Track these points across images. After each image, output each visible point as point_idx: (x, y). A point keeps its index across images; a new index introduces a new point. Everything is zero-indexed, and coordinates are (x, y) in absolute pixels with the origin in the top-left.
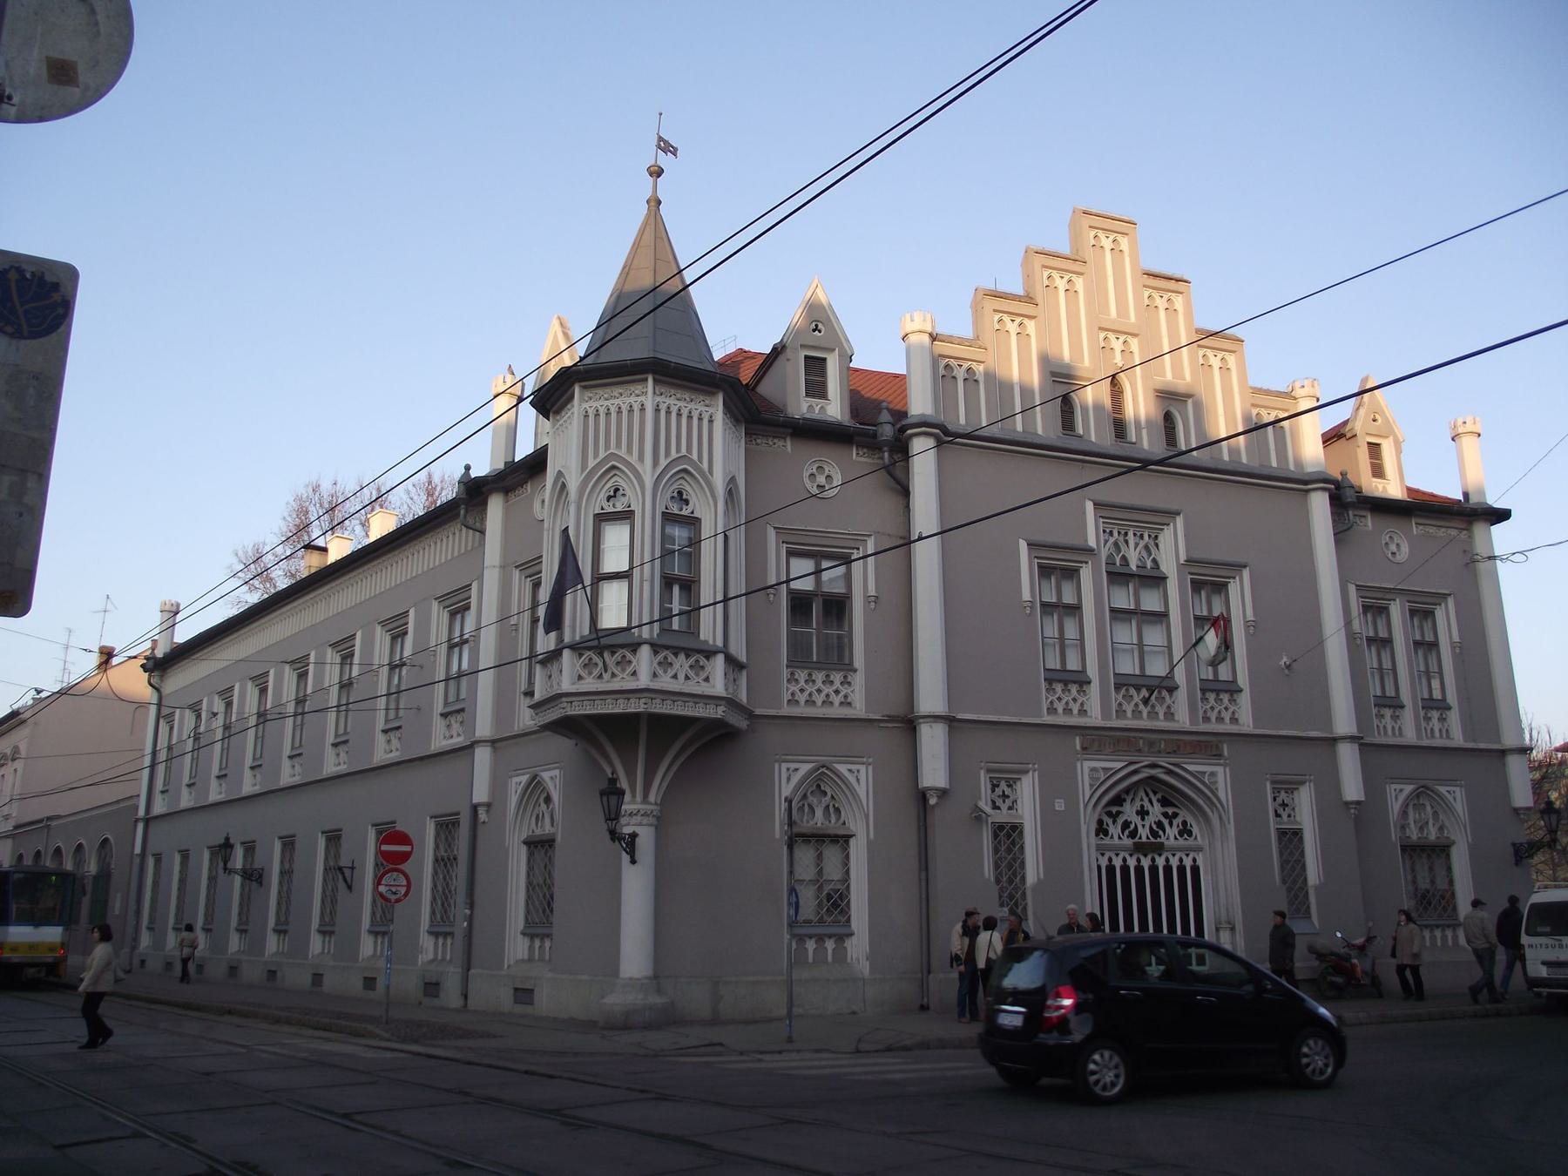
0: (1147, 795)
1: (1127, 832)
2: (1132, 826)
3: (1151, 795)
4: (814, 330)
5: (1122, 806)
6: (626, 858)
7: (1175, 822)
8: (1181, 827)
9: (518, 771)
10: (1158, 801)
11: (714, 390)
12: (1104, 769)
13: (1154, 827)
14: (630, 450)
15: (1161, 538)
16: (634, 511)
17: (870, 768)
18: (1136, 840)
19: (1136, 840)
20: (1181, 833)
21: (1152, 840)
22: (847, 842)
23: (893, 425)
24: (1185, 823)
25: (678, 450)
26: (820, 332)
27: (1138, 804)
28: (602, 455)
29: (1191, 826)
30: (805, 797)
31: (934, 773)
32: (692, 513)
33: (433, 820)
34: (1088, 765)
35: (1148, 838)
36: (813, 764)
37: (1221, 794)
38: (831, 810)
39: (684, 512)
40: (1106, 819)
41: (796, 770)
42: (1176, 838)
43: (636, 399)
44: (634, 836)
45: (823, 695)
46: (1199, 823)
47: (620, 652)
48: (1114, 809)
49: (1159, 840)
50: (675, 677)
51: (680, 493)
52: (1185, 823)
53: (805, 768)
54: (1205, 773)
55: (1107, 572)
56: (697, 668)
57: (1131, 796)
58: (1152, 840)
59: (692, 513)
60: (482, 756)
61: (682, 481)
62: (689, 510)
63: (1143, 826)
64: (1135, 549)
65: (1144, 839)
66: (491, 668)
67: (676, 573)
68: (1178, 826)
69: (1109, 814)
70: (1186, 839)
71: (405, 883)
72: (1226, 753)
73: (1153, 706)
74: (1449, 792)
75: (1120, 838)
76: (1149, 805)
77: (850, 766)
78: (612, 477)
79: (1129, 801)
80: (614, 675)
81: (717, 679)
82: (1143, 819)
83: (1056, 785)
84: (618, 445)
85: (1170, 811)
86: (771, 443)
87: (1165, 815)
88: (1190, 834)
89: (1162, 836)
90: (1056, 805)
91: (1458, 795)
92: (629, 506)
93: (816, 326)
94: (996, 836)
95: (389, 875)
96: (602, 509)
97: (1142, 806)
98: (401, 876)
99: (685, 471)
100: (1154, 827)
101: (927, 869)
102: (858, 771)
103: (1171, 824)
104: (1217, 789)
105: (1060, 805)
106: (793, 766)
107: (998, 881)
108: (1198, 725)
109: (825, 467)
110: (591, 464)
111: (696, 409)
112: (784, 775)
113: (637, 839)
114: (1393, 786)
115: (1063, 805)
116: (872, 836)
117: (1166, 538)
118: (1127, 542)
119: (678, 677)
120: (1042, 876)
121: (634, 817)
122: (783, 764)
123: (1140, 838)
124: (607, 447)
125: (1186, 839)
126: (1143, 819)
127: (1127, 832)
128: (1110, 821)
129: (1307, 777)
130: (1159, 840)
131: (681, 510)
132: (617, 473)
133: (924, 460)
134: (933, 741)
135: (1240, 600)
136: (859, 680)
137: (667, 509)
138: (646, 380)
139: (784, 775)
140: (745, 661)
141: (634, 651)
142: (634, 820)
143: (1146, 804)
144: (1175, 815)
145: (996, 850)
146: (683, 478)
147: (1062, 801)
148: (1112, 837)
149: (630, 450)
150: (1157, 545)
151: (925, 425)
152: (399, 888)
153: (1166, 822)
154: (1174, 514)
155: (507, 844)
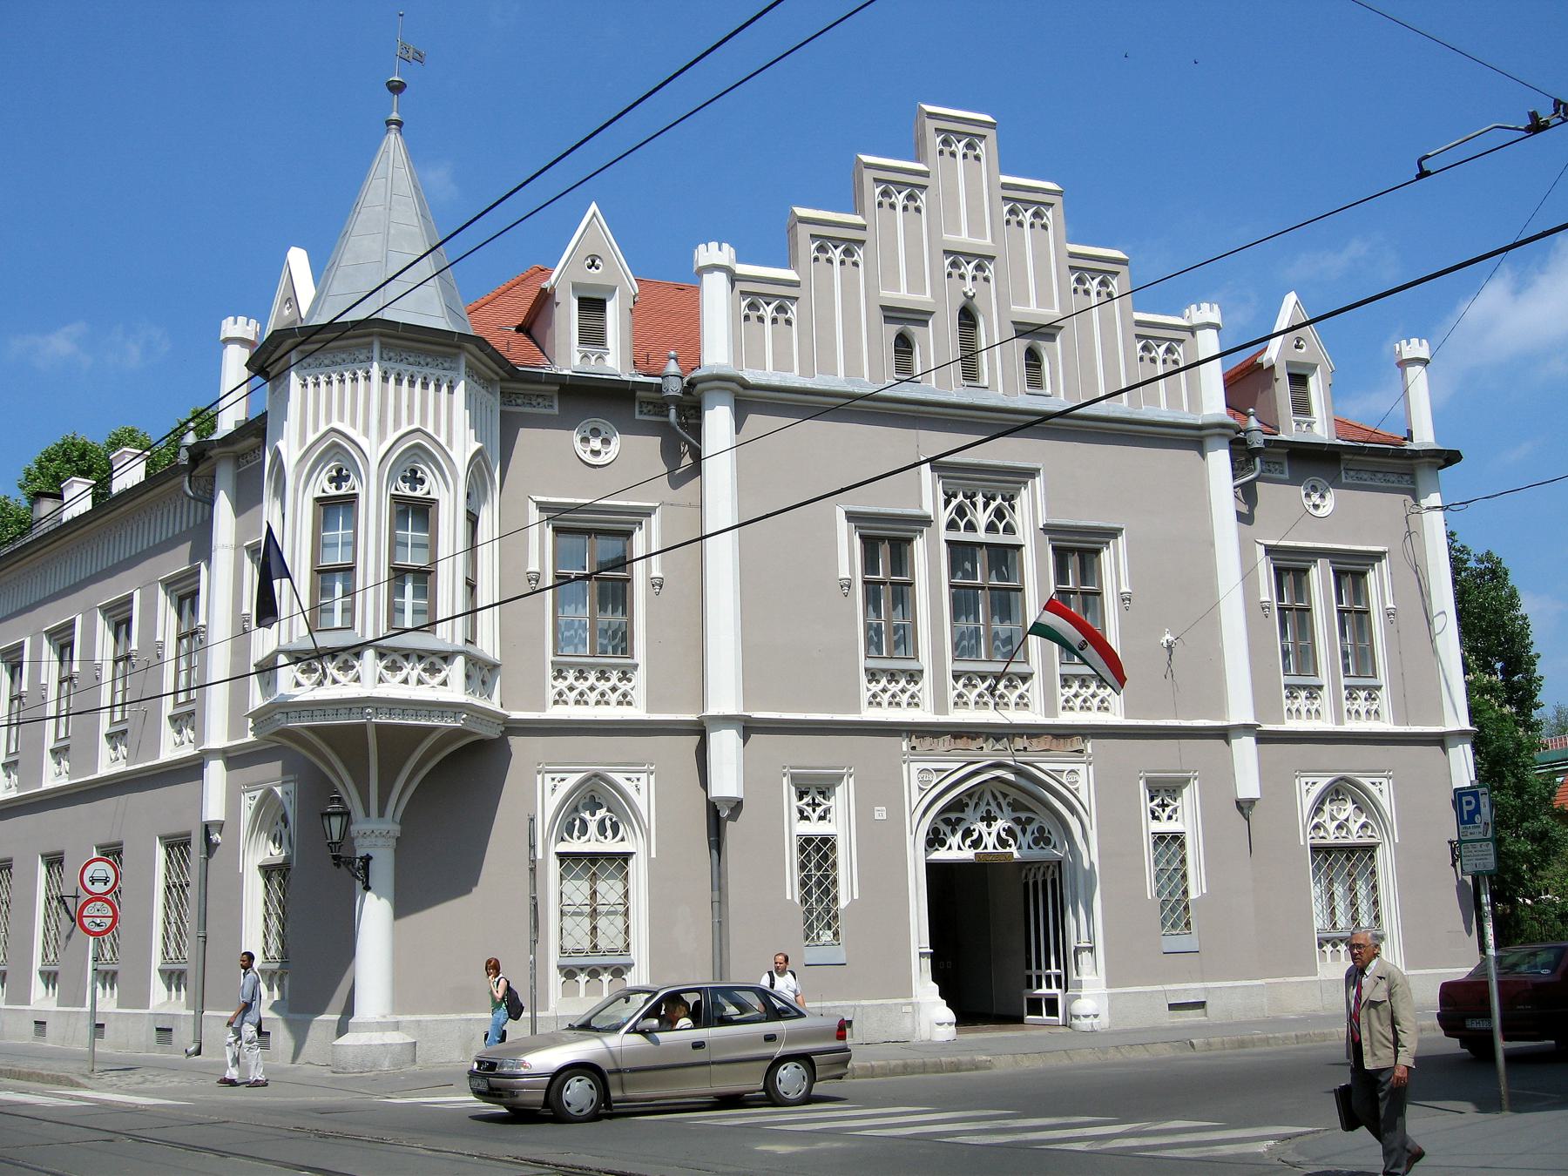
0: (995, 798)
1: (968, 842)
2: (976, 835)
3: (1001, 799)
4: (590, 267)
5: (963, 811)
6: (359, 884)
7: (1029, 829)
8: (1036, 834)
9: (252, 786)
10: (1009, 804)
11: (456, 351)
12: (936, 770)
13: (1003, 835)
14: (354, 424)
15: (1017, 502)
16: (358, 494)
17: (652, 778)
18: (980, 850)
19: (980, 850)
20: (1036, 841)
21: (1001, 850)
22: (626, 861)
23: (682, 378)
24: (1041, 829)
25: (410, 421)
26: (597, 268)
27: (983, 809)
28: (323, 428)
29: (1049, 832)
30: (576, 810)
31: (726, 781)
32: (429, 493)
33: (100, 850)
34: (915, 767)
35: (995, 847)
36: (583, 774)
37: (1083, 796)
38: (608, 823)
39: (418, 493)
40: (943, 827)
41: (1314, 783)
42: (1029, 847)
43: (445, 372)
44: (367, 860)
45: (576, 692)
46: (1058, 832)
47: (343, 656)
48: (953, 816)
49: (1008, 850)
50: (405, 681)
51: (414, 472)
52: (1041, 829)
53: (573, 779)
54: (1063, 771)
55: (946, 541)
56: (346, 667)
57: (975, 800)
58: (1001, 850)
59: (429, 493)
60: (215, 771)
61: (416, 458)
62: (425, 490)
63: (989, 834)
64: (984, 511)
65: (990, 849)
66: (227, 680)
67: (409, 563)
68: (1033, 833)
69: (947, 822)
70: (1042, 848)
71: (110, 913)
72: (1090, 751)
73: (1002, 696)
74: (1374, 784)
75: (959, 848)
76: (998, 811)
77: (1373, 780)
78: (336, 454)
79: (972, 805)
80: (335, 681)
81: (452, 687)
82: (989, 826)
83: (872, 794)
84: (341, 419)
85: (1023, 816)
86: (1273, 469)
87: (1017, 821)
88: (1048, 841)
89: (1013, 845)
90: (876, 814)
91: (1384, 787)
92: (354, 489)
93: (593, 262)
94: (802, 849)
95: (92, 904)
96: (324, 491)
97: (988, 812)
98: (106, 905)
99: (418, 446)
100: (1003, 835)
101: (720, 889)
102: (638, 779)
103: (1024, 831)
104: (1077, 789)
105: (880, 813)
106: (1311, 780)
107: (804, 901)
108: (1056, 715)
109: (1317, 485)
110: (311, 438)
111: (392, 368)
112: (549, 785)
113: (371, 863)
114: (1304, 780)
115: (885, 813)
116: (653, 855)
117: (1023, 500)
118: (974, 505)
119: (406, 686)
120: (856, 897)
121: (369, 839)
122: (546, 775)
123: (986, 847)
124: (329, 420)
125: (1042, 848)
126: (989, 826)
127: (968, 842)
128: (948, 830)
129: (845, 770)
130: (1008, 850)
131: (415, 489)
132: (339, 450)
133: (718, 421)
134: (725, 746)
135: (1114, 568)
136: (639, 677)
137: (397, 489)
138: (371, 344)
139: (1305, 787)
140: (497, 657)
141: (358, 656)
142: (367, 842)
143: (994, 808)
144: (1030, 821)
145: (803, 867)
146: (415, 454)
147: (884, 808)
148: (950, 848)
149: (437, 430)
150: (1013, 508)
151: (722, 381)
152: (104, 920)
153: (1017, 829)
154: (1032, 473)
155: (241, 871)
